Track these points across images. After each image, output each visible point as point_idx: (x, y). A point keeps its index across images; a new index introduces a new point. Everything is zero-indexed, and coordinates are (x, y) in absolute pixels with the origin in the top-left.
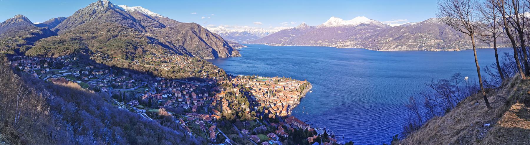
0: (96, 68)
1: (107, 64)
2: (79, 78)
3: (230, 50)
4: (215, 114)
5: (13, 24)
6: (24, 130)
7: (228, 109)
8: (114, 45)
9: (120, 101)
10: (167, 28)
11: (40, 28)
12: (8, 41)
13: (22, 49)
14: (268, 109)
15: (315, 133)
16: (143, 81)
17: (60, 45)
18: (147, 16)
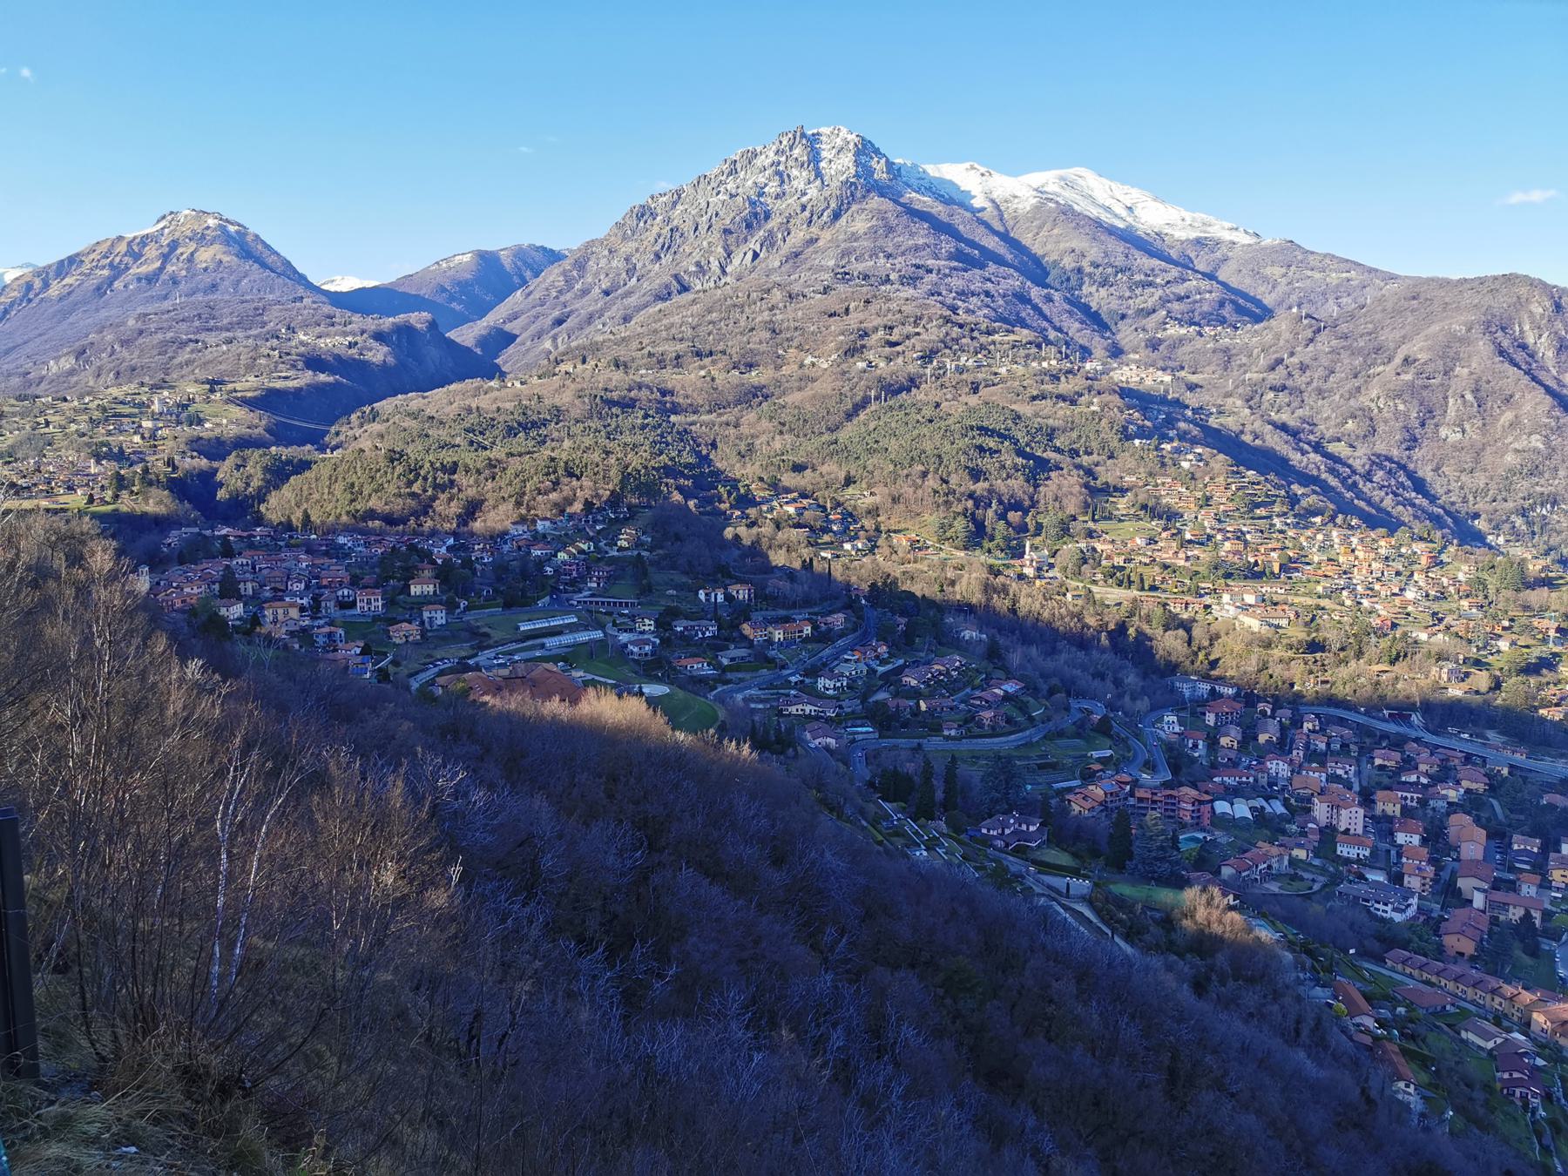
0: (763, 597)
1: (838, 572)
2: (654, 667)
5: (151, 279)
6: (279, 1034)
8: (893, 445)
9: (923, 812)
10: (1281, 324)
11: (371, 323)
12: (110, 415)
13: (231, 477)
16: (1081, 694)
17: (521, 442)
18: (1130, 238)
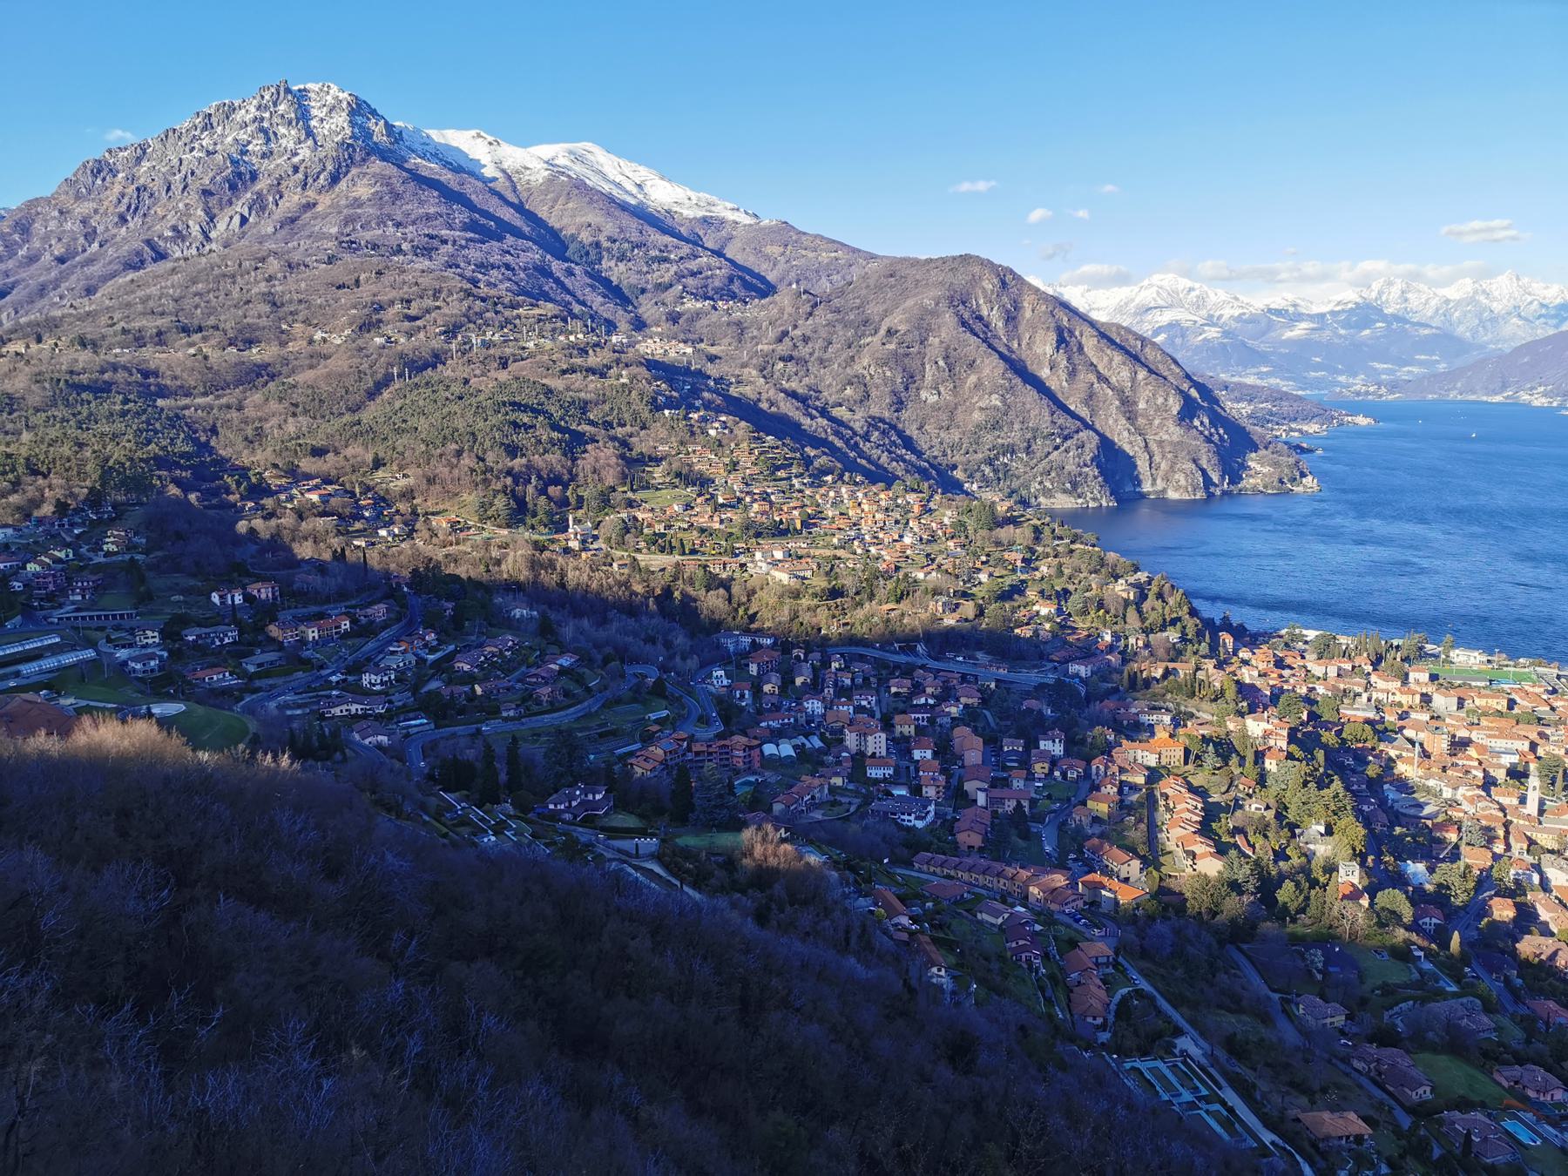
1: (374, 559)
2: (161, 685)
3: (1234, 445)
7: (1201, 847)
8: (423, 424)
9: (488, 798)
14: (1515, 891)
16: (636, 660)
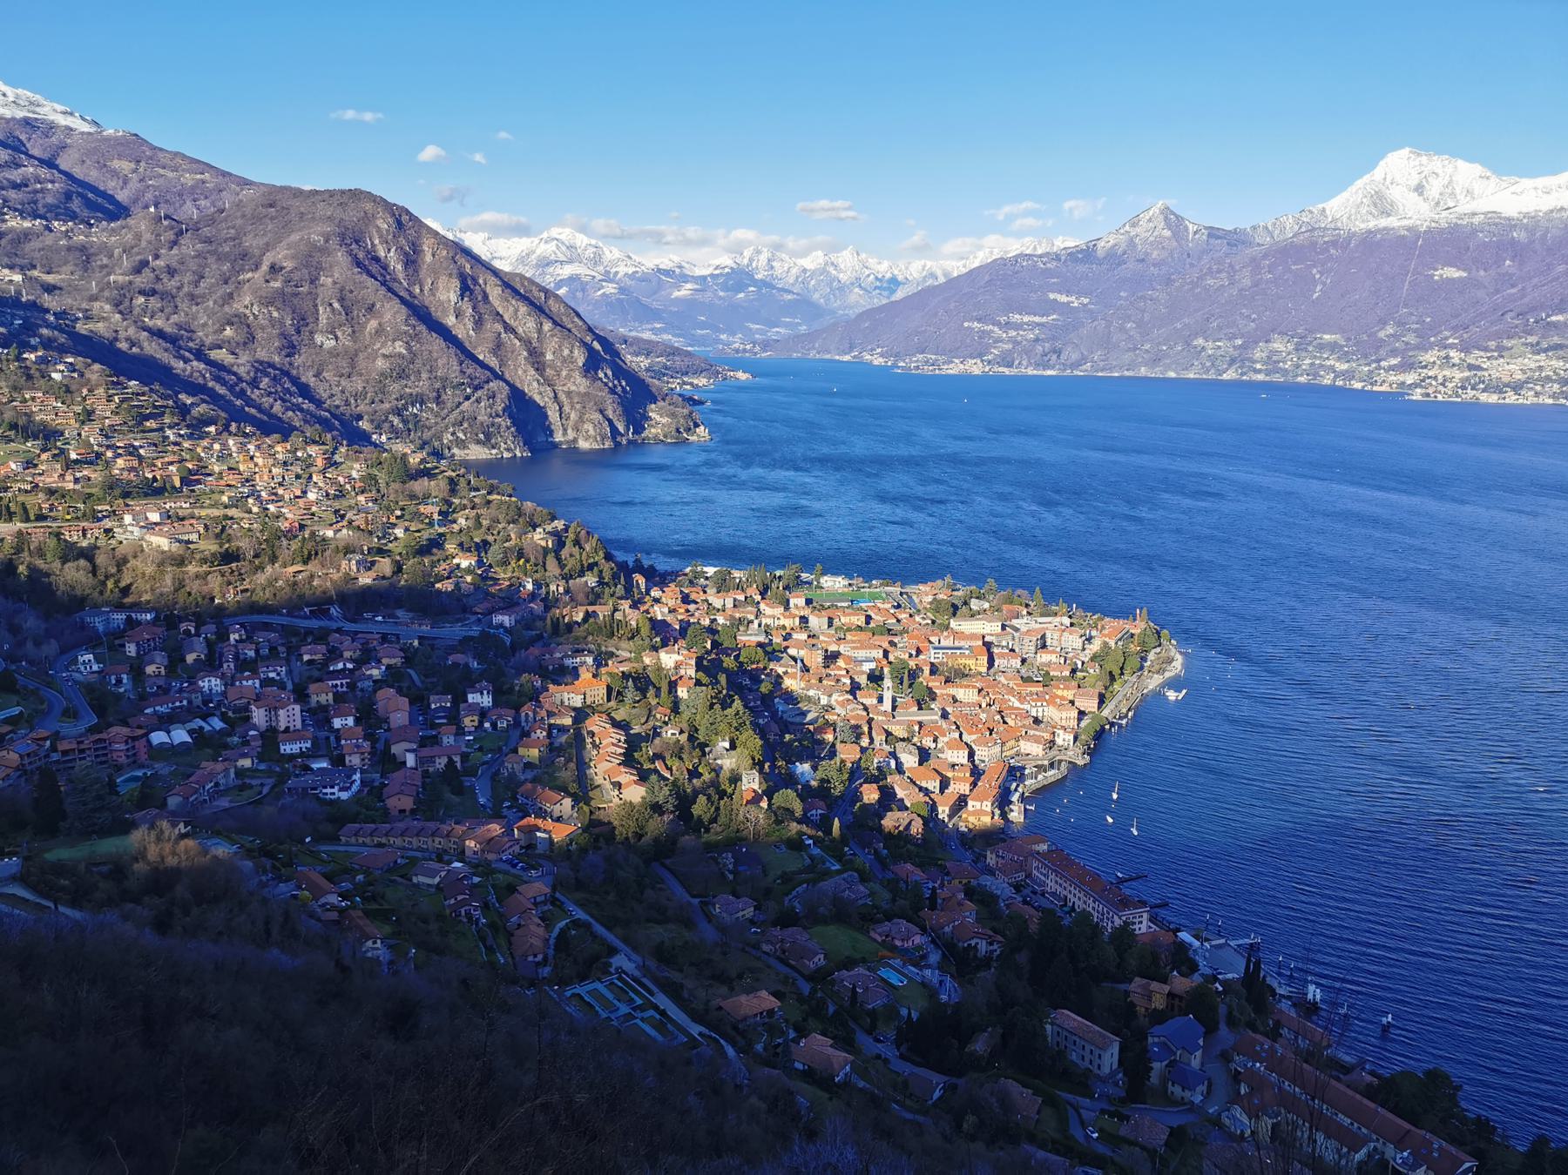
3: (636, 397)
4: (542, 814)
7: (626, 777)
10: (140, 223)
14: (879, 777)
15: (1183, 959)
